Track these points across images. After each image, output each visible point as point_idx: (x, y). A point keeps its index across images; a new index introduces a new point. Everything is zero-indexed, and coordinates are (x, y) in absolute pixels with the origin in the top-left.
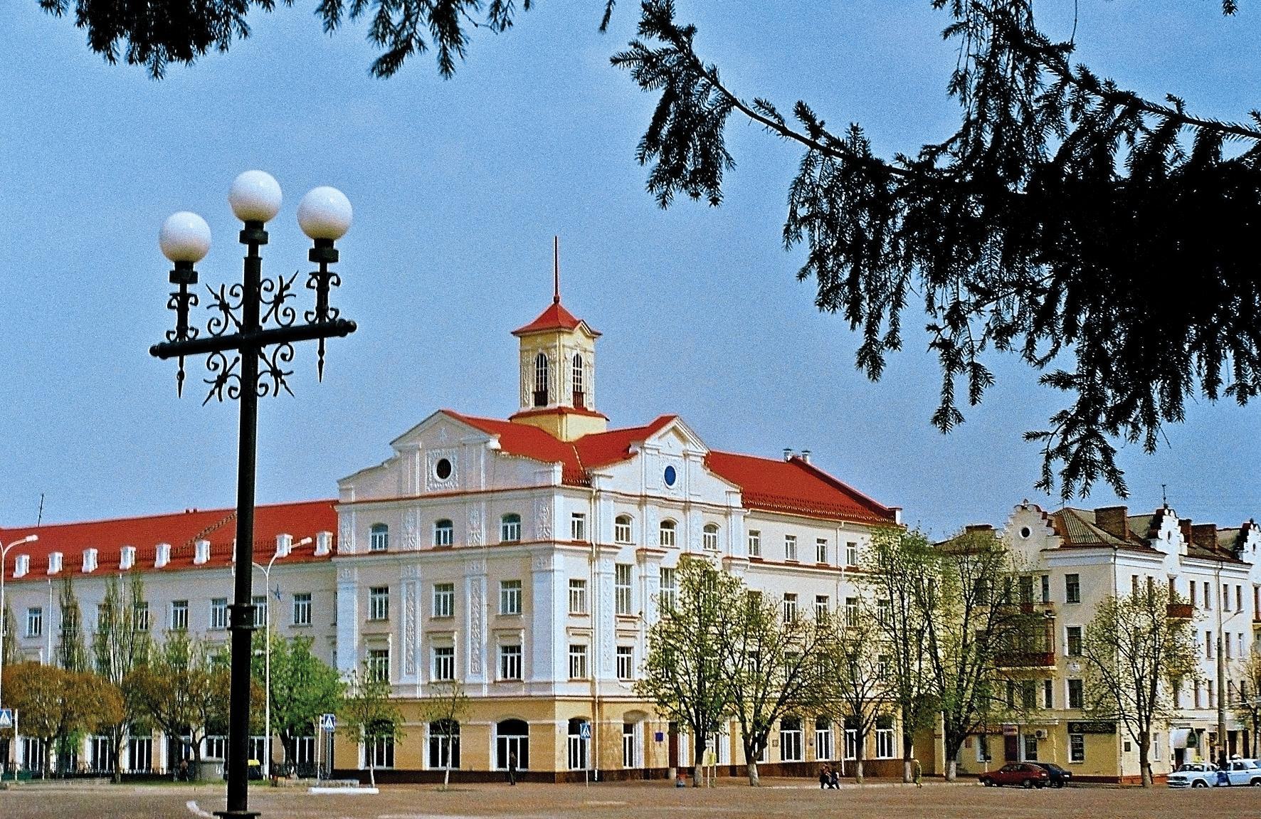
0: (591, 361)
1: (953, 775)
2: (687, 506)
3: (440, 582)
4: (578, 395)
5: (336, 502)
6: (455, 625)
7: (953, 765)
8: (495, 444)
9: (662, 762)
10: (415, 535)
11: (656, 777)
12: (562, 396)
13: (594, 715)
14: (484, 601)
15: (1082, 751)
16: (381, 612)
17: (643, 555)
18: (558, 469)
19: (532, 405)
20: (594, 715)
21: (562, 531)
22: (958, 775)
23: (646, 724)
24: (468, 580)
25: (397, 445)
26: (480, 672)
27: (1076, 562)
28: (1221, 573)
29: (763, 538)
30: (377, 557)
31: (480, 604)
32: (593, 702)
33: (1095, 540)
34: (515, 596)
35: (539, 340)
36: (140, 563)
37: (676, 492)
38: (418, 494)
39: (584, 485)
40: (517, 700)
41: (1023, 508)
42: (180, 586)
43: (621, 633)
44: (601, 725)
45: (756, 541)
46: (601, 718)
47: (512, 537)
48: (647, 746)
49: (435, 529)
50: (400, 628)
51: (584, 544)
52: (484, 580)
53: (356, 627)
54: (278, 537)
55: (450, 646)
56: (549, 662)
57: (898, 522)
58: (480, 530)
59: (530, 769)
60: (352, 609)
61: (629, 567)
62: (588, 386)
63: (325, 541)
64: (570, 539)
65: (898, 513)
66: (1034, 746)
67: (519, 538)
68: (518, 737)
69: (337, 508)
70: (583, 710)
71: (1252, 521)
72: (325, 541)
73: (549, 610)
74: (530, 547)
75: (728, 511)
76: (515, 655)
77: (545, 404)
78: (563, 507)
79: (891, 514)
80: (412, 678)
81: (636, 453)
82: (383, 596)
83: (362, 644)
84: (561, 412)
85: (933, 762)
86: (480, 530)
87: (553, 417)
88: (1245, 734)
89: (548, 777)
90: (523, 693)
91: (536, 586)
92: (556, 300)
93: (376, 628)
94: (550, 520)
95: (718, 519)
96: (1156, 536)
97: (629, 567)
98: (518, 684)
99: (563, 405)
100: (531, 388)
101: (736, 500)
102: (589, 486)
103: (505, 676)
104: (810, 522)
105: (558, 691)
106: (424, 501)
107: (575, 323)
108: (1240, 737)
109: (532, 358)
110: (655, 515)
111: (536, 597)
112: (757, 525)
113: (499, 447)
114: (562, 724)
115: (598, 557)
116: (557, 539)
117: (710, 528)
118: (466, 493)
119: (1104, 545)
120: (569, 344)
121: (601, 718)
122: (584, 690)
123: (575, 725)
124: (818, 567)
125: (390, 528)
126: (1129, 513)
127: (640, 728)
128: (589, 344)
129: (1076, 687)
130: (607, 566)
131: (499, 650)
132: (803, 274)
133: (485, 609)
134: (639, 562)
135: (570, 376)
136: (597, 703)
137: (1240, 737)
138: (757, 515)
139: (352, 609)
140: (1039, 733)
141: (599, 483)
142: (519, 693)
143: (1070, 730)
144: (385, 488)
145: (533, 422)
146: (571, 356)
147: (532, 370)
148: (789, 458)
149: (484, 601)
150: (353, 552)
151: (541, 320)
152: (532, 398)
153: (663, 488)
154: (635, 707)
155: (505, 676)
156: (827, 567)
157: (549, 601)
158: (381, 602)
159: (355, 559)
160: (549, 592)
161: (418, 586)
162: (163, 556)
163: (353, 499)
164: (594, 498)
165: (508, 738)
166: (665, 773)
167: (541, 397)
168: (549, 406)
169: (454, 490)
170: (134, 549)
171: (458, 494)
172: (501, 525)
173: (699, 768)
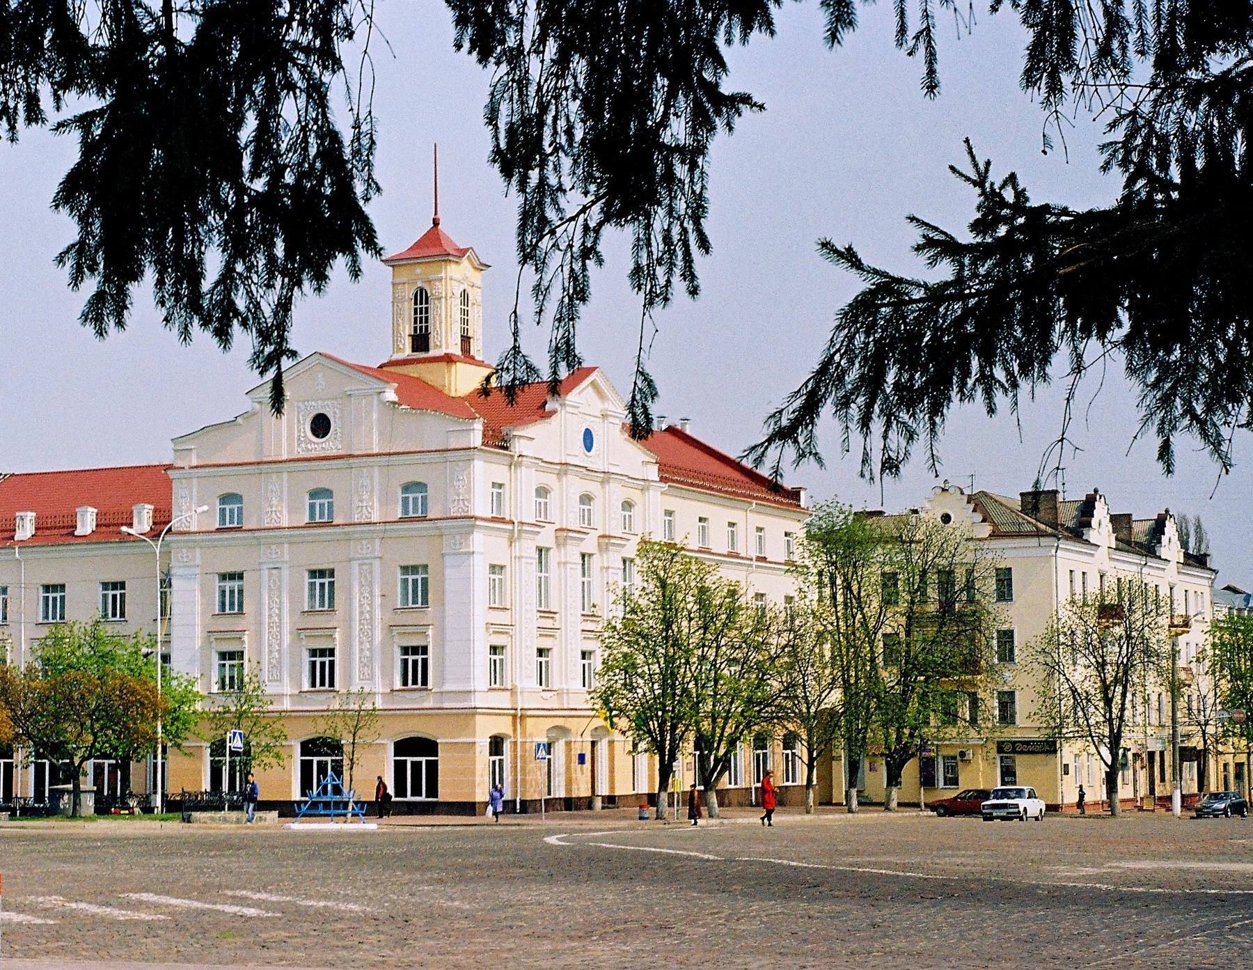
0: (479, 299)
1: (854, 803)
2: (606, 477)
3: (314, 568)
4: (466, 339)
5: (170, 467)
6: (335, 620)
7: (854, 792)
8: (390, 395)
9: (583, 791)
10: (280, 506)
11: (578, 808)
12: (445, 340)
13: (515, 730)
14: (377, 592)
15: (1014, 774)
16: (232, 604)
17: (563, 534)
18: (478, 426)
19: (407, 352)
20: (515, 730)
21: (481, 507)
22: (860, 804)
23: (568, 744)
24: (355, 565)
25: (253, 395)
26: (371, 678)
27: (1011, 553)
28: (1145, 570)
29: (677, 518)
30: (225, 535)
31: (371, 593)
32: (514, 716)
33: (1028, 528)
34: (418, 585)
35: (418, 271)
36: (39, 533)
37: (595, 460)
38: (284, 457)
39: (503, 448)
40: (330, 715)
41: (944, 490)
42: (56, 564)
43: (544, 632)
44: (523, 743)
45: (670, 521)
46: (524, 733)
47: (415, 510)
48: (568, 768)
49: (307, 501)
50: (260, 624)
51: (502, 521)
52: (377, 563)
53: (198, 620)
54: (135, 509)
55: (238, 649)
56: (467, 666)
57: (802, 504)
58: (371, 500)
59: (440, 799)
60: (192, 602)
61: (548, 549)
62: (475, 331)
63: (146, 516)
64: (490, 516)
65: (802, 493)
66: (954, 769)
67: (425, 509)
68: (423, 759)
69: (172, 474)
70: (502, 726)
71: (1167, 511)
72: (146, 516)
73: (468, 603)
74: (440, 524)
75: (644, 485)
76: (327, 660)
77: (427, 350)
78: (485, 470)
79: (795, 494)
80: (282, 684)
81: (554, 412)
82: (235, 584)
83: (207, 642)
84: (448, 359)
85: (831, 786)
86: (371, 500)
87: (435, 365)
88: (1162, 753)
89: (468, 808)
90: (430, 705)
91: (449, 572)
92: (436, 223)
93: (225, 624)
94: (469, 491)
95: (635, 495)
96: (1089, 525)
97: (548, 549)
98: (424, 693)
99: (450, 351)
100: (407, 329)
101: (653, 473)
102: (506, 448)
103: (314, 685)
104: (721, 501)
105: (478, 701)
106: (291, 464)
107: (463, 252)
108: (1157, 758)
109: (409, 293)
110: (575, 486)
111: (449, 586)
112: (673, 503)
113: (396, 399)
114: (483, 744)
115: (519, 538)
116: (477, 514)
117: (628, 505)
118: (351, 456)
119: (1039, 534)
120: (457, 275)
121: (524, 733)
122: (503, 700)
123: (496, 745)
124: (730, 555)
125: (245, 498)
126: (1060, 498)
127: (559, 748)
128: (477, 277)
129: (1006, 699)
130: (527, 549)
131: (215, 657)
132: (988, 163)
133: (378, 600)
134: (558, 545)
135: (457, 316)
136: (519, 717)
137: (1157, 758)
138: (674, 492)
139: (192, 602)
140: (962, 754)
141: (518, 447)
142: (425, 705)
143: (1000, 750)
144: (240, 449)
145: (411, 370)
146: (458, 292)
147: (408, 308)
148: (664, 427)
149: (377, 592)
150: (193, 529)
151: (418, 245)
152: (408, 343)
153: (582, 455)
154: (560, 722)
155: (314, 685)
156: (737, 556)
157: (467, 590)
158: (232, 592)
159: (198, 537)
160: (468, 579)
161: (285, 573)
162: (87, 522)
163: (194, 463)
164: (514, 463)
165: (409, 760)
166: (589, 803)
167: (421, 341)
168: (432, 353)
169: (334, 453)
170: (34, 514)
171: (341, 457)
172: (400, 496)
173: (664, 796)
